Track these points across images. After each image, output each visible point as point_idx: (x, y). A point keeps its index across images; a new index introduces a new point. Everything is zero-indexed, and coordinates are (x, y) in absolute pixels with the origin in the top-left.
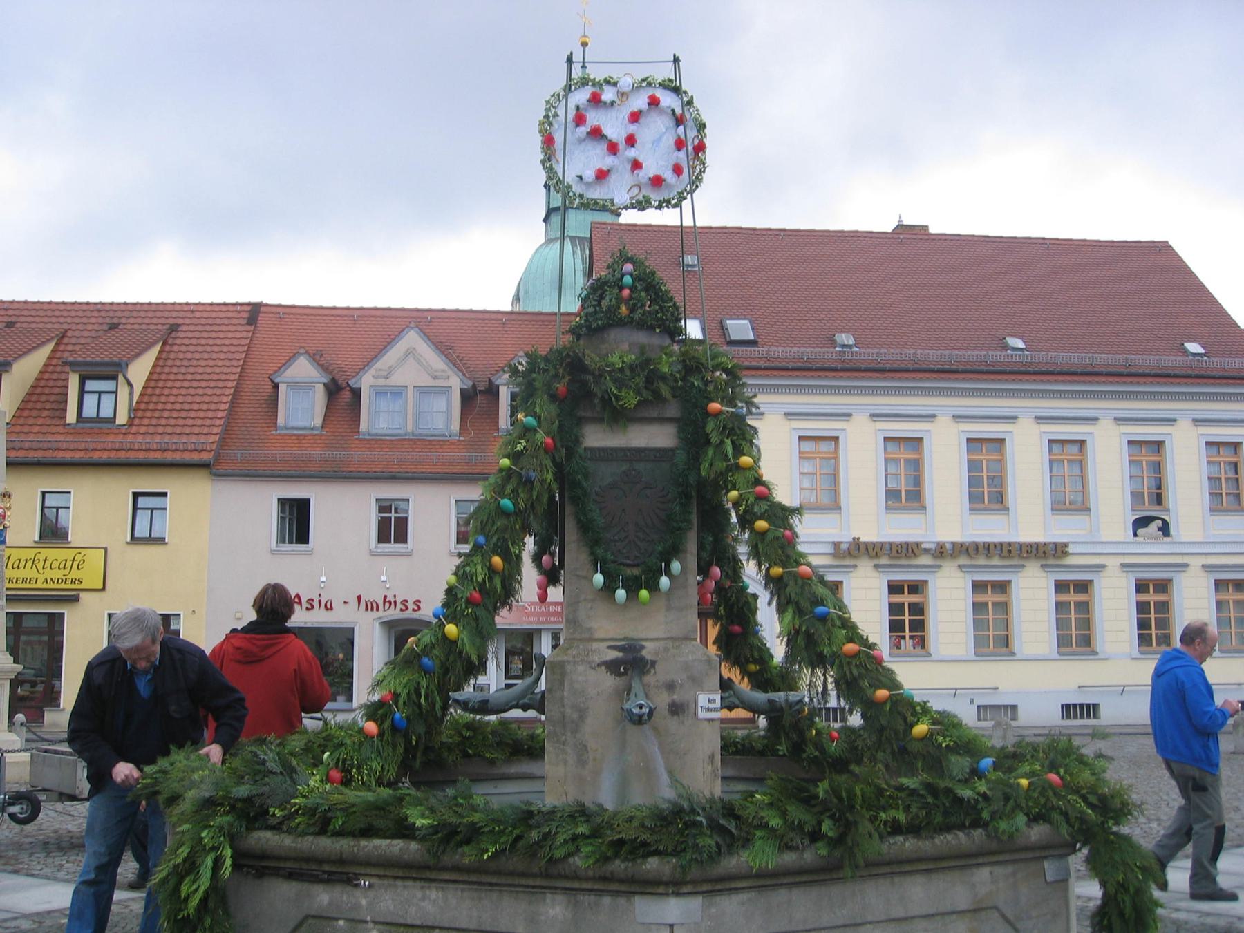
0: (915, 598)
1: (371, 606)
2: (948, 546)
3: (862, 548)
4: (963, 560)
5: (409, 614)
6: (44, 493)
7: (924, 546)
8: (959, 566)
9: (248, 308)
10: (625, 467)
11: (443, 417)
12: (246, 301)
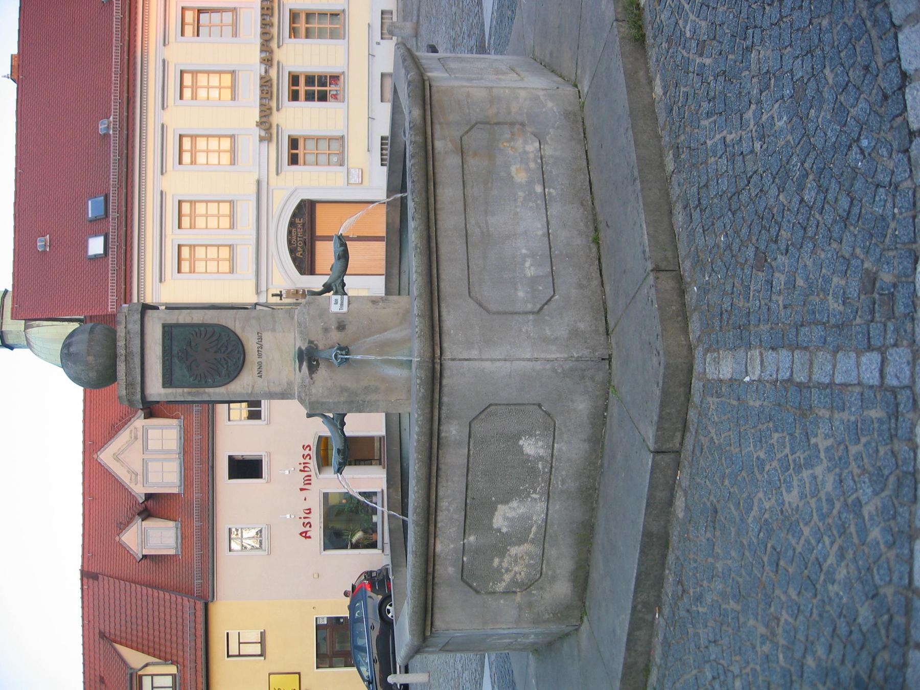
0: (302, 81)
1: (308, 481)
2: (264, 55)
3: (264, 119)
4: (274, 45)
5: (313, 453)
6: (228, 656)
7: (263, 73)
8: (279, 47)
9: (85, 580)
10: (176, 360)
11: (165, 435)
12: (79, 582)
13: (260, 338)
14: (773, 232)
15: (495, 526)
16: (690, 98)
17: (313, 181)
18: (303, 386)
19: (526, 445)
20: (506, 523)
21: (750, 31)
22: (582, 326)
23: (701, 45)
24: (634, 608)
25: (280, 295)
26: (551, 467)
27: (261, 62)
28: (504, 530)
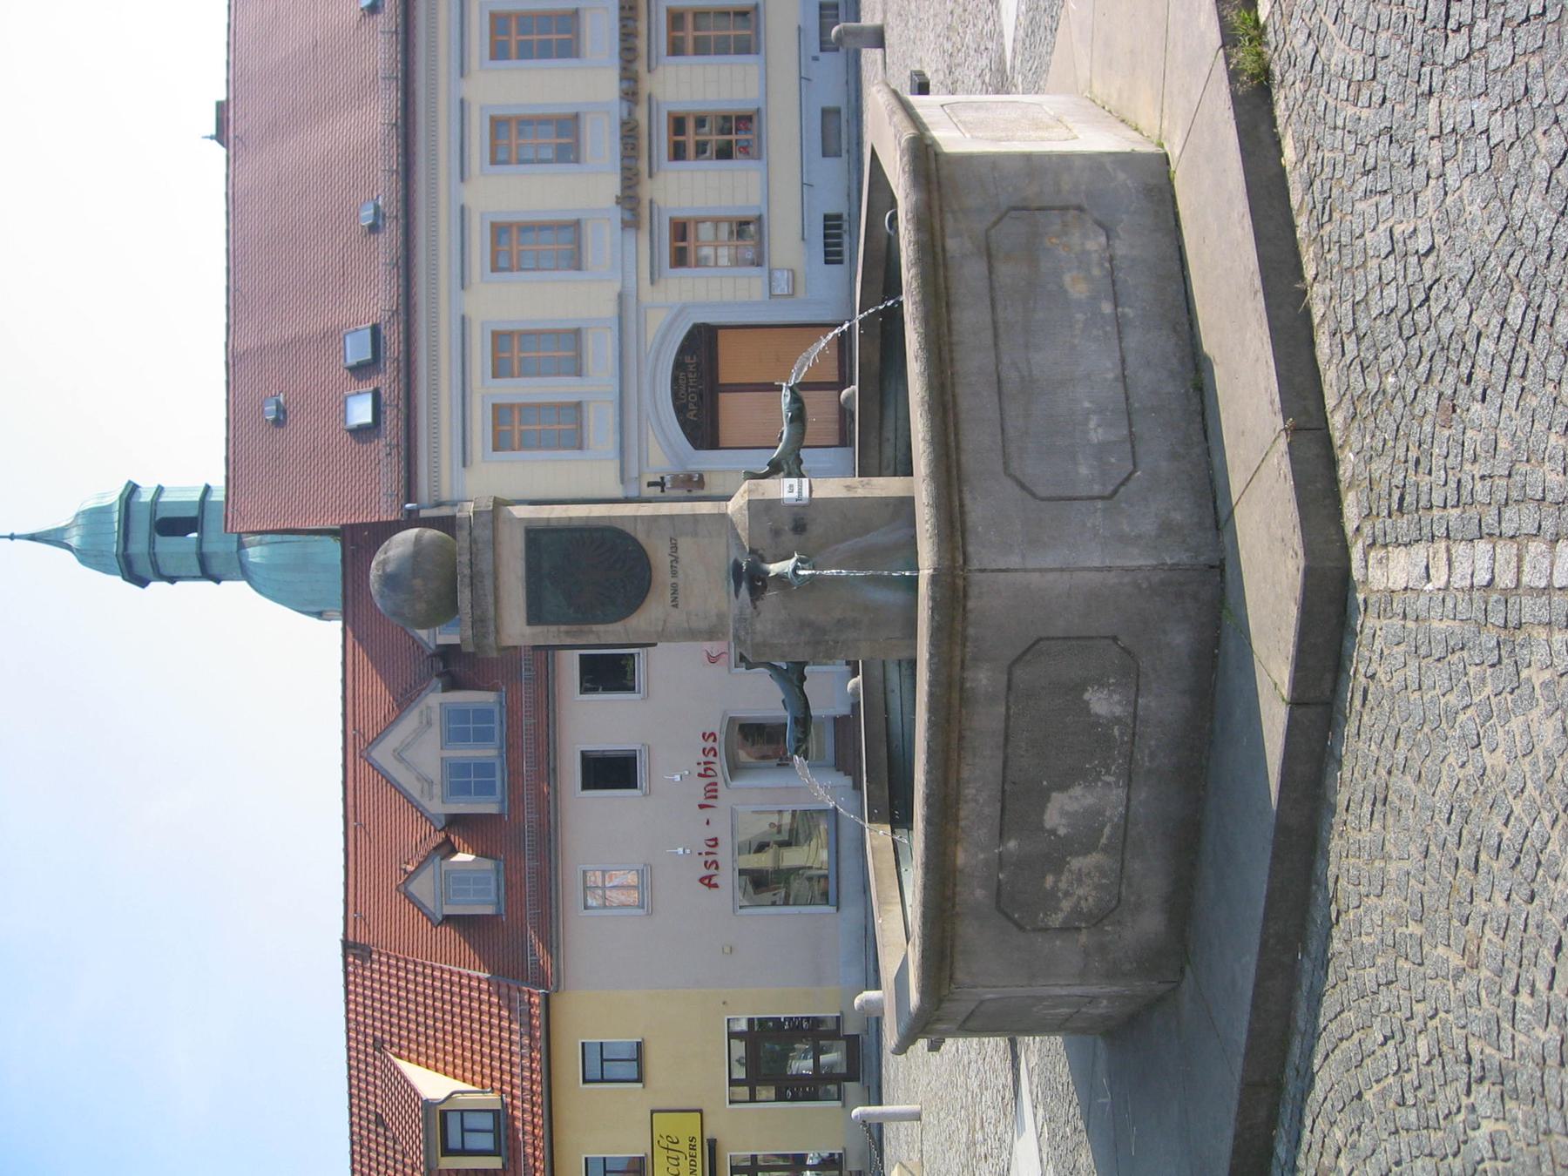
1: (712, 792)
3: (629, 193)
4: (641, 66)
5: (720, 747)
6: (585, 1081)
13: (674, 547)
14: (1464, 370)
15: (1048, 825)
16: (1339, 167)
17: (719, 291)
18: (741, 619)
19: (1094, 699)
20: (1064, 821)
21: (1426, 70)
22: (1177, 516)
23: (1355, 86)
24: (1264, 945)
25: (661, 484)
26: (1134, 734)
27: (622, 98)
28: (1062, 831)
